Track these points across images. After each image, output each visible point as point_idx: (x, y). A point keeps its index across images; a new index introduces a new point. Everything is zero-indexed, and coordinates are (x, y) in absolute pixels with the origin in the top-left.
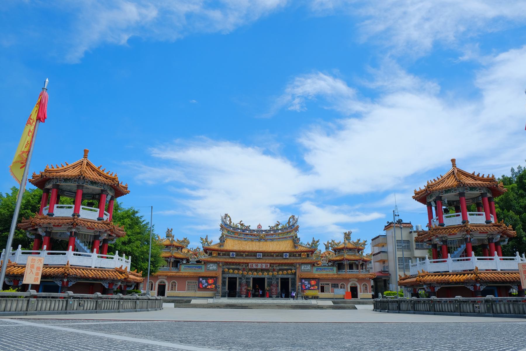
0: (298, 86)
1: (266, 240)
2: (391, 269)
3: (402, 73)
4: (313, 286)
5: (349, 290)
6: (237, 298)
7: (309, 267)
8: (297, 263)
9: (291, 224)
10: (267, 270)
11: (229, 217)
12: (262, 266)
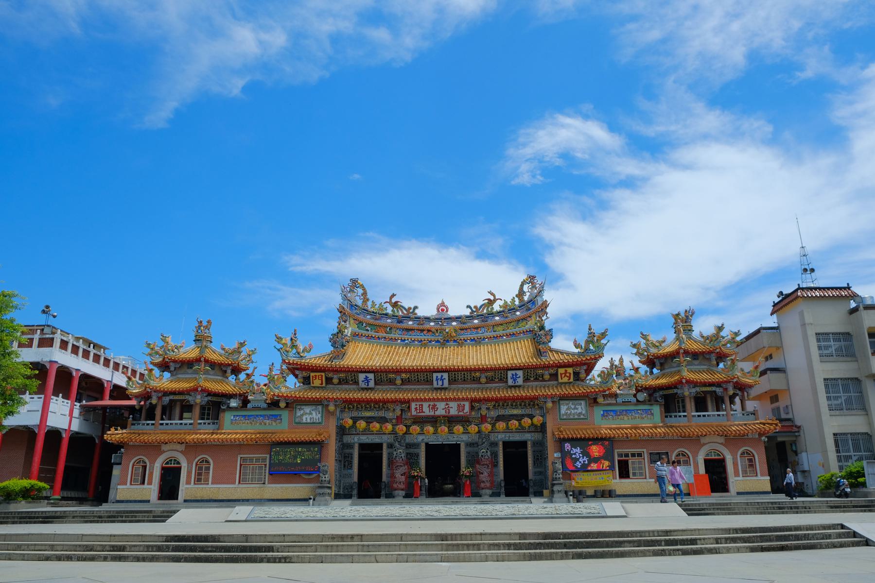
0: (524, 145)
1: (460, 343)
2: (801, 414)
3: (699, 107)
4: (596, 460)
5: (702, 470)
6: (383, 500)
7: (581, 408)
8: (546, 397)
9: (526, 298)
11: (362, 286)
12: (447, 409)
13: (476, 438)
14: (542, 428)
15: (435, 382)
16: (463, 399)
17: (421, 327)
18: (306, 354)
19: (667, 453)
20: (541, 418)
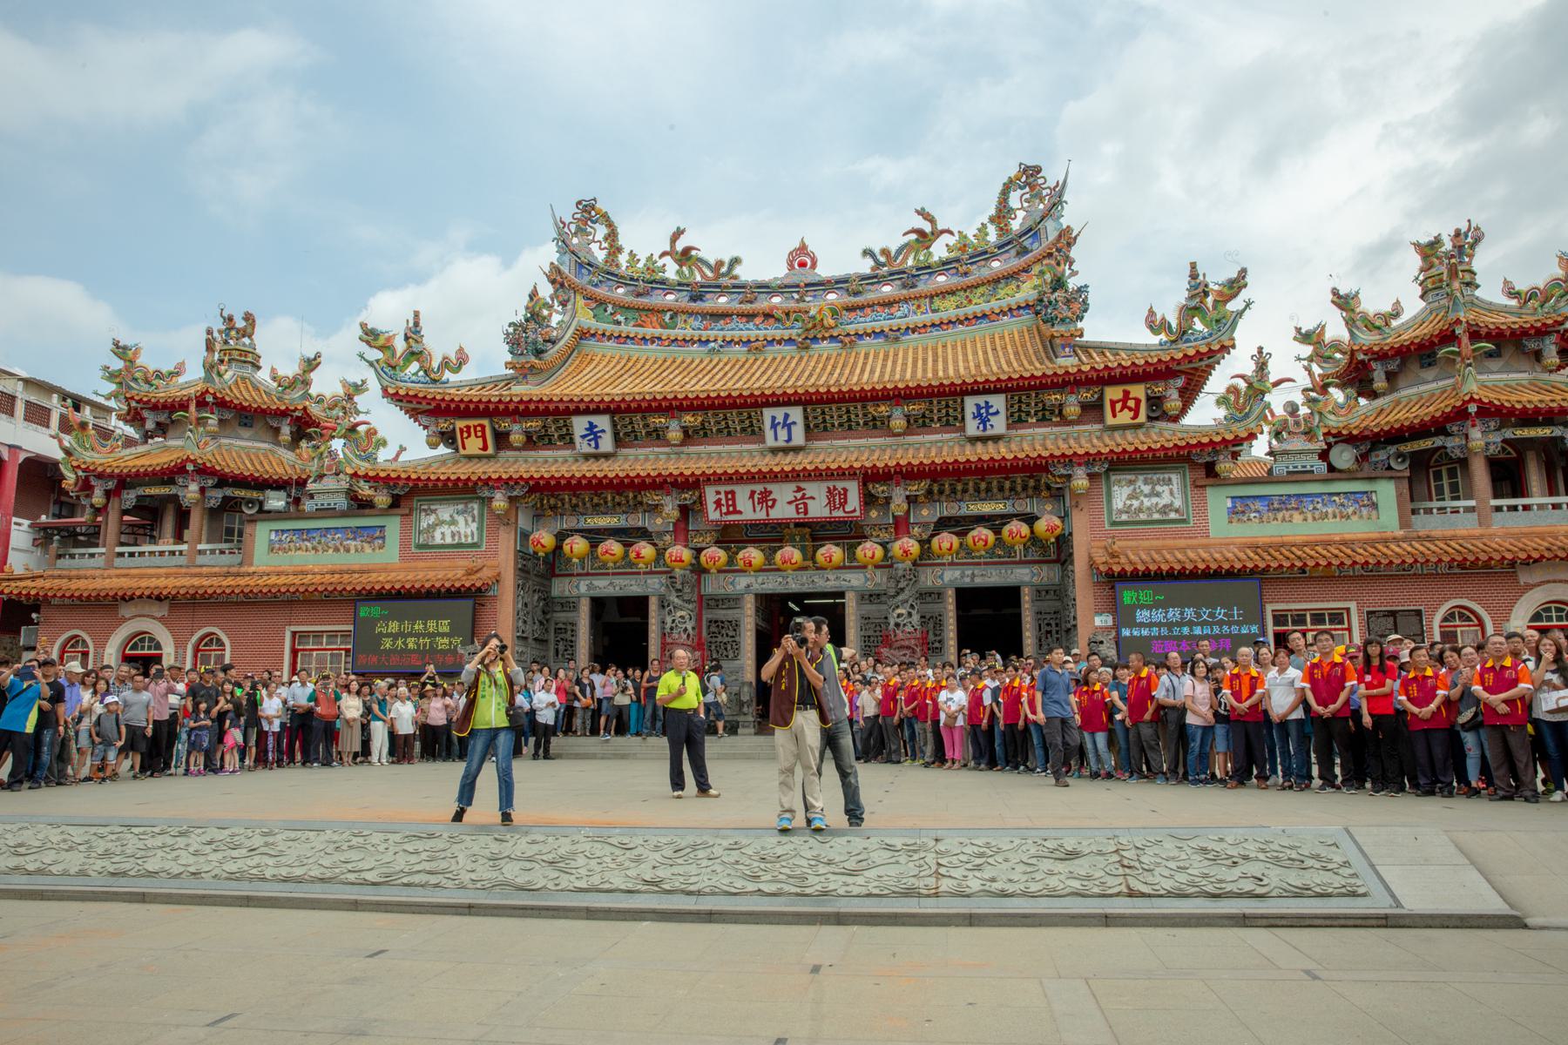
8: (1069, 460)
9: (1016, 225)
10: (848, 533)
12: (801, 502)
13: (879, 579)
14: (1059, 551)
15: (769, 434)
16: (842, 474)
17: (747, 307)
18: (447, 375)
19: (1419, 613)
20: (1058, 522)
